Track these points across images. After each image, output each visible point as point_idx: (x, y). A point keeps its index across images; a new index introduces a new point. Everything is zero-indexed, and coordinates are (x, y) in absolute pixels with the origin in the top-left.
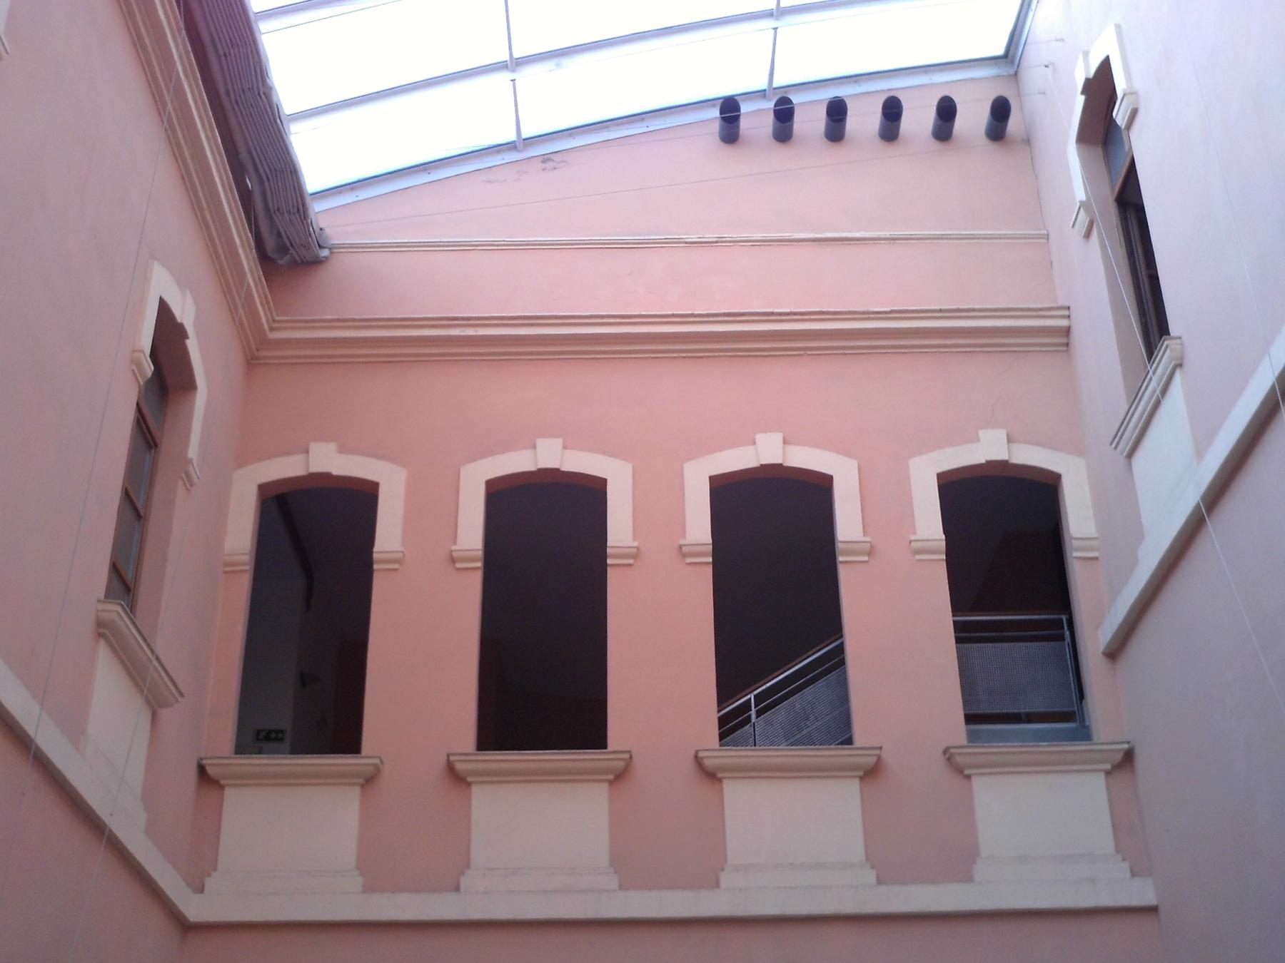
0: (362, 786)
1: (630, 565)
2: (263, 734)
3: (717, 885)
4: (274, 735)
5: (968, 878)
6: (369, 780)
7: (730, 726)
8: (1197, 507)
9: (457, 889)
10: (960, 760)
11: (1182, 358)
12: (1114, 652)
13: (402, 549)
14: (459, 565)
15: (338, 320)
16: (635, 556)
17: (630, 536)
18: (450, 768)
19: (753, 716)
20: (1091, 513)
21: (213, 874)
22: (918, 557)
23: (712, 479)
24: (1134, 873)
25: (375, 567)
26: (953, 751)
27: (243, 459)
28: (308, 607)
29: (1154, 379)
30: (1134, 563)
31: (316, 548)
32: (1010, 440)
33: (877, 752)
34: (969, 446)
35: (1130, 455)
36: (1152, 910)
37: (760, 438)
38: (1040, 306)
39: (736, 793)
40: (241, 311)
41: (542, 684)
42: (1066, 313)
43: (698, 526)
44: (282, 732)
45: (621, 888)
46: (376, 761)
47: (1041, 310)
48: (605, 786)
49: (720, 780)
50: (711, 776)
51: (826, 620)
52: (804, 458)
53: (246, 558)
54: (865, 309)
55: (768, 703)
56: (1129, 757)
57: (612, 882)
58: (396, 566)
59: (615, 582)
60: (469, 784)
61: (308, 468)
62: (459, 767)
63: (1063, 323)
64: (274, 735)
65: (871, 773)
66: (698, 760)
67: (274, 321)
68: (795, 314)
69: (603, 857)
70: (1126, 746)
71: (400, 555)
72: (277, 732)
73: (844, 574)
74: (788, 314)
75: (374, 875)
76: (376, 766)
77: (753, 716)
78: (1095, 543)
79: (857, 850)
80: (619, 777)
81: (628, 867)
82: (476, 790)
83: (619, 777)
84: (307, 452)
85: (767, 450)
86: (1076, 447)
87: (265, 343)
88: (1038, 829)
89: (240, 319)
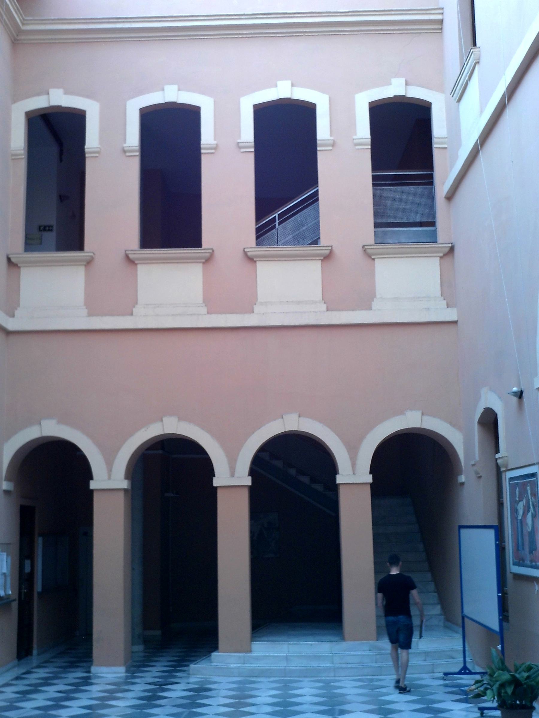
0: (86, 266)
1: (213, 153)
2: (42, 228)
3: (252, 311)
4: (47, 228)
5: (369, 308)
6: (89, 263)
7: (262, 233)
8: (476, 143)
9: (132, 314)
10: (369, 251)
11: (479, 59)
12: (450, 197)
13: (99, 146)
14: (128, 154)
15: (58, 19)
16: (215, 149)
17: (213, 138)
18: (127, 257)
19: (277, 225)
20: (445, 123)
21: (18, 309)
22: (357, 147)
23: (255, 106)
24: (448, 306)
25: (87, 155)
26: (366, 247)
27: (16, 99)
28: (61, 160)
29: (467, 68)
30: (456, 157)
31: (57, 137)
32: (407, 84)
33: (330, 248)
34: (386, 87)
35: (459, 100)
36: (456, 322)
37: (279, 83)
38: (427, 8)
39: (262, 267)
40: (4, 17)
41: (171, 214)
42: (441, 11)
43: (247, 133)
44: (52, 226)
45: (208, 313)
46: (92, 254)
47: (428, 10)
48: (201, 265)
49: (255, 262)
50: (251, 260)
51: (311, 177)
52: (302, 94)
53: (23, 152)
54: (335, 11)
55: (284, 217)
56: (452, 249)
57: (204, 310)
58: (97, 155)
59: (205, 162)
60: (136, 264)
61: (49, 102)
62: (131, 256)
63: (439, 17)
64: (47, 228)
65: (328, 257)
66: (245, 253)
67: (24, 19)
68: (299, 13)
69: (200, 300)
70: (450, 245)
71: (99, 149)
72: (49, 226)
73: (320, 156)
74: (295, 13)
75: (93, 307)
76: (91, 256)
77: (277, 225)
78: (446, 139)
79: (319, 295)
80: (208, 260)
81: (211, 304)
82: (139, 267)
83: (208, 260)
84: (48, 94)
85: (282, 90)
86: (440, 89)
87: (20, 32)
88: (406, 284)
89: (5, 21)
